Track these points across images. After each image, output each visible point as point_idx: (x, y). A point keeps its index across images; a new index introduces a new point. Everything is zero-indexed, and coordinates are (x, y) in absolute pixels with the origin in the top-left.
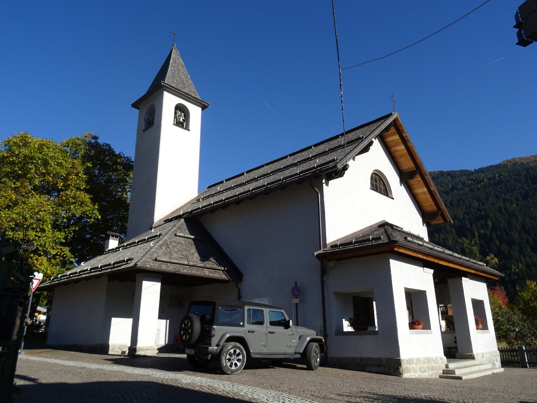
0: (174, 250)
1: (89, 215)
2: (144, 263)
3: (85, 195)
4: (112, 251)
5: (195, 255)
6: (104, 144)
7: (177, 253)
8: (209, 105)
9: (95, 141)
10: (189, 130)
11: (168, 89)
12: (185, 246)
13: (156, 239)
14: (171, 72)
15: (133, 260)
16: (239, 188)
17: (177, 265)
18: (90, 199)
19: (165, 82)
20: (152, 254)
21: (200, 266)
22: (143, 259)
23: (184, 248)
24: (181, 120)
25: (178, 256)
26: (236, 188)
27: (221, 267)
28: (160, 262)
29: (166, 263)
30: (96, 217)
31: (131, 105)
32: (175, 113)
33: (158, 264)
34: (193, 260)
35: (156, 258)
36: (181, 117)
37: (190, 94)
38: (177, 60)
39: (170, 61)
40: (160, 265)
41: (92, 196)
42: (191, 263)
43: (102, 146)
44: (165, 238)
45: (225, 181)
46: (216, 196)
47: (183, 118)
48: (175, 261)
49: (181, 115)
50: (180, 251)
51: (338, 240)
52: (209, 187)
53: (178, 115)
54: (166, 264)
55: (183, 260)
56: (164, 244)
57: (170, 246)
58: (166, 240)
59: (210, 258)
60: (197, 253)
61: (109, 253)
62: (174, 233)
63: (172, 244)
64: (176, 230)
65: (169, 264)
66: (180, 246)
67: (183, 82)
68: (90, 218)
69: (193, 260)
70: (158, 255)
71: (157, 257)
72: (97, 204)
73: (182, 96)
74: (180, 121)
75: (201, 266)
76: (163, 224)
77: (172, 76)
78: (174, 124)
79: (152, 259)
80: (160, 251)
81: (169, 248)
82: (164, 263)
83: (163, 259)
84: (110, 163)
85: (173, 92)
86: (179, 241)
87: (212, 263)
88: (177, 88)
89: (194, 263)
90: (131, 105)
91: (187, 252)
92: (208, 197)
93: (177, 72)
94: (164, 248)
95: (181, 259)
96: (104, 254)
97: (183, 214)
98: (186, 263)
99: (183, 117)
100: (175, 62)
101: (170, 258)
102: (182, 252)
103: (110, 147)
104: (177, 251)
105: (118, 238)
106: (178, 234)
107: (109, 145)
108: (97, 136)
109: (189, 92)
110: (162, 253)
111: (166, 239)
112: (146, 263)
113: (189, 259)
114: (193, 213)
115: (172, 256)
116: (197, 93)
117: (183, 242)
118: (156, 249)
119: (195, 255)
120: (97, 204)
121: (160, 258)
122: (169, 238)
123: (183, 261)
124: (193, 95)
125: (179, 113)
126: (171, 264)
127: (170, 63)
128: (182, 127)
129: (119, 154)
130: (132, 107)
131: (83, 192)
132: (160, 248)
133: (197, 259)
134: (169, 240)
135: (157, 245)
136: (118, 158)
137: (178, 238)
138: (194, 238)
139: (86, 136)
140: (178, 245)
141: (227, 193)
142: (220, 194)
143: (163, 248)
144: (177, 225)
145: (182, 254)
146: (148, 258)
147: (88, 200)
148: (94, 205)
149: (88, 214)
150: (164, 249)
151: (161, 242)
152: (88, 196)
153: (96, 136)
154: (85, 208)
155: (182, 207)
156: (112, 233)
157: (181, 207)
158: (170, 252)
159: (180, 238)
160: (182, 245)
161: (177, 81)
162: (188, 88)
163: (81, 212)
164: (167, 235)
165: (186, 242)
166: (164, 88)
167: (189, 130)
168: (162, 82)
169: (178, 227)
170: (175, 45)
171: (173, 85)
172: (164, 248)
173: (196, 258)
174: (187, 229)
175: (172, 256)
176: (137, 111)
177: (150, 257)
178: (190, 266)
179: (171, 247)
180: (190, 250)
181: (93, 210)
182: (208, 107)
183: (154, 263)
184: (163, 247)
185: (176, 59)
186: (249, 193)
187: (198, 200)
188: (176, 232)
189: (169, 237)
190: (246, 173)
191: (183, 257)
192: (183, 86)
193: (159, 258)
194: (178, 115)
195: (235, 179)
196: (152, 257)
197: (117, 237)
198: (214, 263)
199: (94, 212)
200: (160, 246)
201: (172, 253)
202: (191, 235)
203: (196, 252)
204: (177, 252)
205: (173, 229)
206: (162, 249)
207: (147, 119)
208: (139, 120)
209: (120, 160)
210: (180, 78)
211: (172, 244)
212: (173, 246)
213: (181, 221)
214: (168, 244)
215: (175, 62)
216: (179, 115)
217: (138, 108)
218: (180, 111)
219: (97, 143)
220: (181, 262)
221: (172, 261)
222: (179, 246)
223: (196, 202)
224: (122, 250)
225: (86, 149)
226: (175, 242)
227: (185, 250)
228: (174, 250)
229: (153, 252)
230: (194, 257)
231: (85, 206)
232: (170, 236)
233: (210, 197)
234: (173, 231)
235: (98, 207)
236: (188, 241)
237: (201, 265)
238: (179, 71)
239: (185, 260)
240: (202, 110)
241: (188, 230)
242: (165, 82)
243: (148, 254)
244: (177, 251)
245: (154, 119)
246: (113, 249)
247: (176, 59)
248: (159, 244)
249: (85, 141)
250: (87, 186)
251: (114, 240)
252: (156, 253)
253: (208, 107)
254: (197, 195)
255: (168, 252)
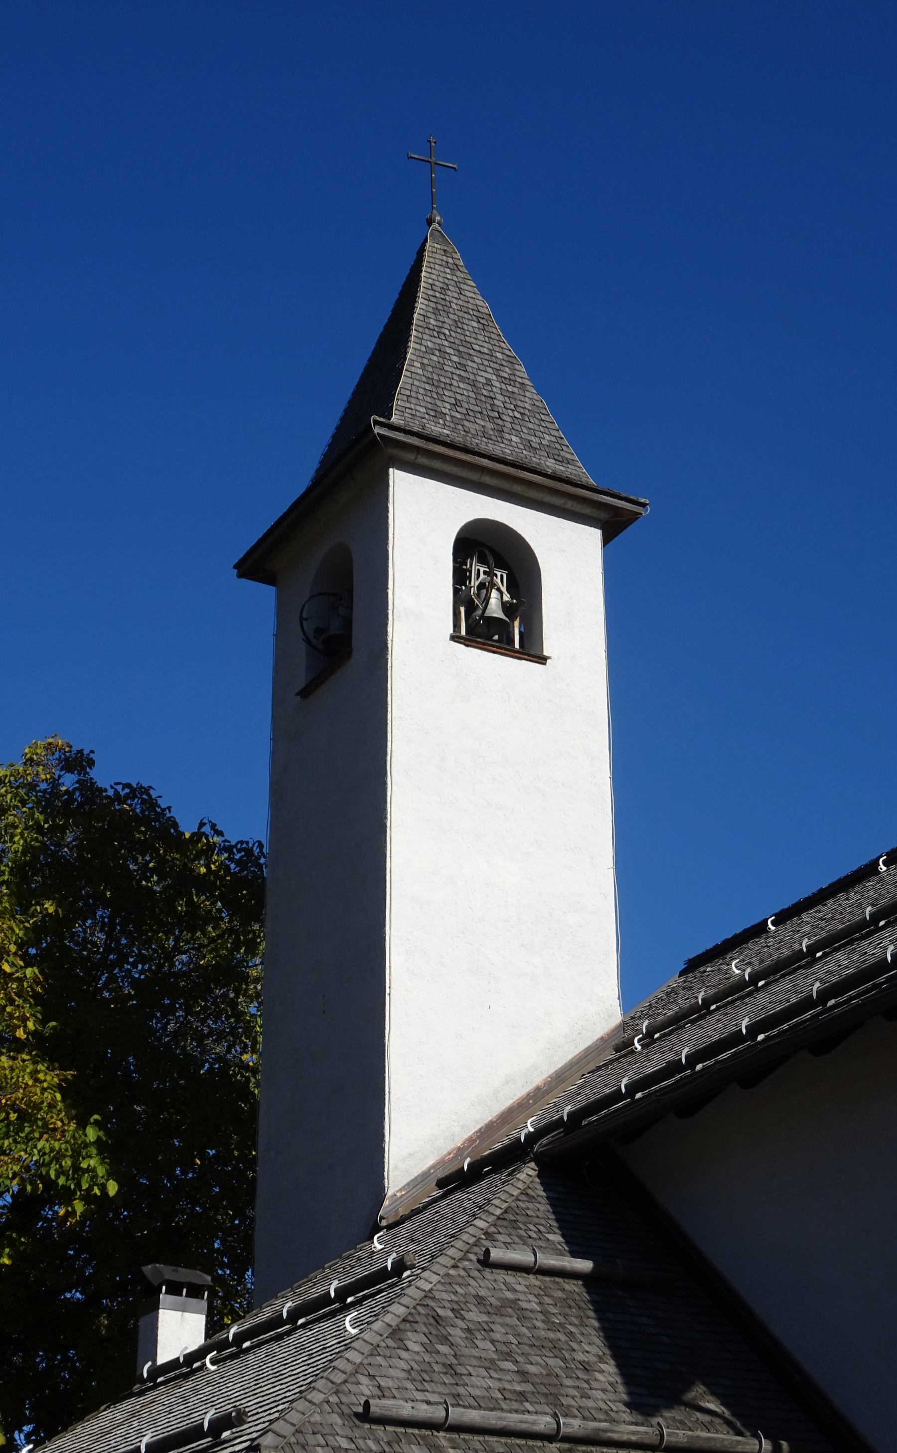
0: (475, 1352)
1: (62, 1181)
2: (299, 1436)
3: (34, 1073)
4: (172, 1374)
5: (602, 1372)
6: (119, 788)
7: (490, 1366)
8: (644, 505)
9: (77, 782)
10: (542, 660)
11: (410, 456)
12: (539, 1324)
13: (380, 1291)
14: (422, 364)
15: (243, 1422)
16: (839, 955)
17: (487, 1438)
18: (60, 1088)
19: (395, 419)
20: (345, 1381)
21: (625, 1437)
22: (294, 1417)
23: (539, 1338)
24: (494, 608)
25: (498, 1385)
26: (825, 956)
27: (758, 1437)
28: (390, 1429)
29: (428, 1433)
30: (96, 1191)
31: (235, 567)
32: (460, 576)
33: (377, 1441)
34: (590, 1403)
35: (367, 1405)
36: (494, 594)
37: (535, 460)
38: (452, 293)
39: (413, 308)
40: (389, 1443)
41: (70, 1074)
42: (573, 1425)
43: (111, 800)
44: (421, 1284)
45: (773, 923)
46: (717, 1016)
47: (507, 597)
48: (474, 1416)
49: (493, 585)
50: (508, 1355)
51: (459, 1152)
52: (693, 965)
53: (474, 583)
54: (422, 1437)
55: (528, 1406)
56: (417, 1318)
57: (450, 1330)
58: (429, 1295)
59: (688, 1386)
60: (612, 1362)
61: (156, 1386)
62: (476, 1249)
63: (463, 1319)
64: (486, 1234)
65: (442, 1434)
66: (513, 1327)
67: (493, 405)
68: (66, 1196)
69: (590, 1403)
70: (379, 1387)
71: (371, 1401)
72: (96, 1117)
73: (487, 480)
74: (488, 613)
75: (634, 1438)
76: (435, 1201)
77: (430, 381)
78: (455, 638)
79: (342, 1415)
80: (395, 1362)
81: (445, 1339)
82: (416, 1431)
83: (405, 1410)
84: (155, 884)
85: (437, 464)
86: (509, 1295)
87: (706, 1418)
88: (459, 439)
89: (592, 1425)
90: (235, 567)
91: (552, 1362)
92: (677, 1022)
93: (455, 359)
94: (414, 1342)
95: (515, 1405)
96: (132, 1395)
97: (539, 1133)
98: (544, 1423)
99: (504, 589)
100: (440, 308)
101: (445, 1402)
102: (519, 1359)
103: (151, 804)
104: (495, 1356)
105: (203, 1298)
106: (496, 1254)
107: (147, 790)
108: (85, 752)
109: (525, 456)
110: (403, 1375)
111: (430, 1291)
112: (311, 1439)
113: (565, 1401)
114: (584, 1123)
115: (461, 1390)
116: (569, 453)
117: (532, 1298)
118: (367, 1349)
119: (602, 1372)
120: (96, 1117)
121: (392, 1402)
122: (448, 1281)
123: (527, 1417)
124: (550, 465)
125: (477, 571)
126: (455, 1436)
127: (415, 316)
128: (504, 647)
129: (198, 836)
130: (240, 576)
131: (29, 1053)
132: (390, 1343)
133: (612, 1396)
134: (445, 1296)
135: (377, 1326)
136: (198, 857)
137: (500, 1278)
138: (594, 1268)
139: (31, 760)
140: (498, 1319)
141: (774, 988)
142: (738, 1003)
143: (410, 1345)
144: (496, 1202)
145: (523, 1375)
146: (319, 1405)
147: (54, 1099)
148: (82, 1124)
149: (53, 1174)
150: (416, 1348)
151: (398, 1310)
152: (50, 1078)
153: (80, 752)
154: (35, 1146)
155: (537, 1095)
156: (168, 1272)
157: (528, 1096)
158: (450, 1366)
159: (509, 1278)
160: (523, 1316)
161: (457, 404)
162: (518, 434)
163: (16, 1168)
164: (435, 1268)
165: (547, 1300)
166: (395, 452)
167: (542, 660)
168: (376, 423)
169: (498, 1212)
170: (438, 218)
171: (435, 429)
172: (414, 1342)
173: (604, 1391)
174: (555, 1224)
175: (461, 1390)
176: (267, 593)
177: (334, 1399)
178: (567, 1439)
179: (459, 1332)
180: (574, 1345)
181: (76, 1155)
182: (635, 516)
183: (357, 1433)
184: (410, 1334)
185: (444, 290)
186: (881, 979)
187: (623, 1047)
188: (487, 1243)
189: (448, 1275)
190: (884, 863)
191: (528, 1387)
192: (490, 426)
193: (385, 1402)
194: (474, 583)
195: (830, 902)
196: (344, 1399)
197: (195, 1292)
198: (717, 1421)
199: (84, 1165)
200: (396, 1333)
201: (461, 1370)
202: (574, 1254)
203: (607, 1351)
204: (492, 1361)
205: (471, 1230)
206: (407, 1349)
207: (318, 631)
208: (280, 635)
209: (208, 867)
210: (473, 384)
211: (463, 1319)
212: (469, 1330)
213: (522, 1176)
214: (437, 1319)
215: (440, 308)
216: (481, 586)
217: (270, 580)
218: (482, 561)
219: (88, 788)
220: (513, 1420)
221: (457, 1415)
222: (502, 1325)
223: (611, 1062)
224: (213, 1368)
225: (38, 828)
226: (480, 1300)
227: (539, 1345)
228: (475, 1352)
229: (349, 1368)
230: (594, 1385)
231: (37, 1135)
232: (455, 1267)
233: (683, 1027)
234: (472, 1240)
235: (101, 1134)
236: (560, 1294)
237: (634, 1433)
238: (464, 350)
239: (539, 1408)
240: (606, 540)
241: (560, 1228)
242: (395, 419)
243: (320, 1384)
244: (495, 1356)
245: (348, 623)
246: (174, 1364)
247: (444, 290)
248: (388, 1318)
249: (32, 787)
250: (43, 1022)
251: (184, 1310)
252: (372, 1377)
253: (635, 516)
254: (616, 1017)
255: (437, 1368)
